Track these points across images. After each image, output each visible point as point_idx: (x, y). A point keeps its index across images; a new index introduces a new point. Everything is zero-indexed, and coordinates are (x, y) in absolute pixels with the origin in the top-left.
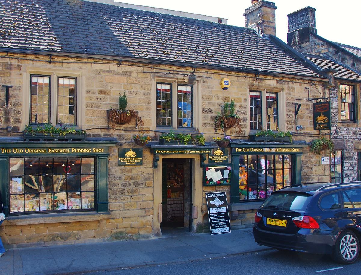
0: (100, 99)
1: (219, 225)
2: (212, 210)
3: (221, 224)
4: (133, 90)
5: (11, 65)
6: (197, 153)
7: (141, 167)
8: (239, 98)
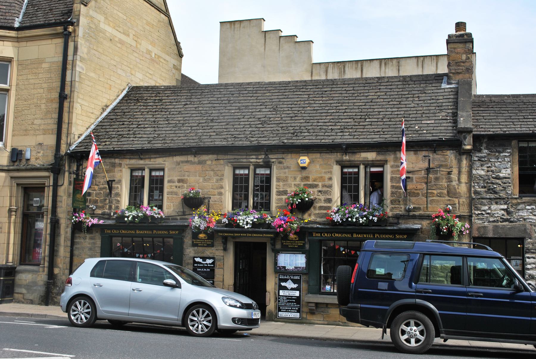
0: (179, 187)
1: (288, 310)
2: (282, 293)
3: (290, 308)
4: (207, 177)
5: (115, 163)
6: (268, 237)
7: (213, 248)
8: (322, 177)
